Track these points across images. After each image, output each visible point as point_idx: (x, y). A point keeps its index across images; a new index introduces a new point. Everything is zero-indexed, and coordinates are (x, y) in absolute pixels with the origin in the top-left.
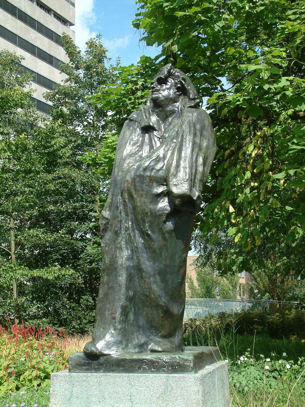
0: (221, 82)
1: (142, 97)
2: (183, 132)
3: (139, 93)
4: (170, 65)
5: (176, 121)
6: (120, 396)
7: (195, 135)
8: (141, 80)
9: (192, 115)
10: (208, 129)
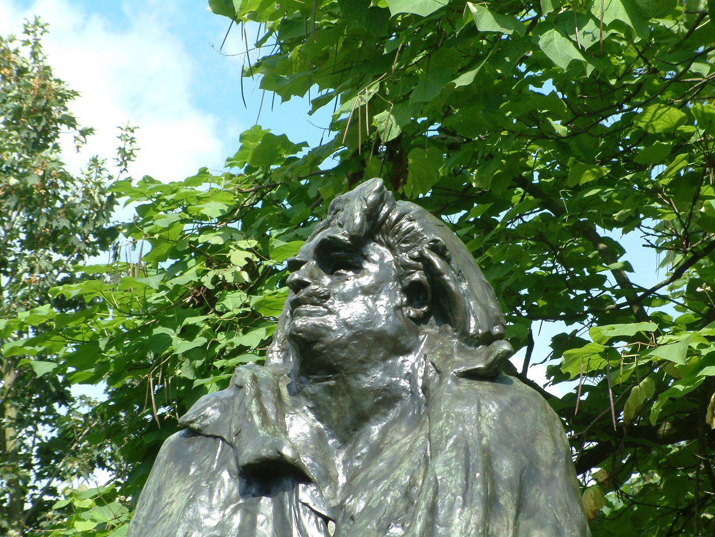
0: (622, 251)
1: (250, 320)
2: (436, 493)
3: (233, 302)
4: (378, 183)
5: (402, 439)
7: (491, 504)
8: (243, 244)
9: (477, 414)
10: (552, 478)
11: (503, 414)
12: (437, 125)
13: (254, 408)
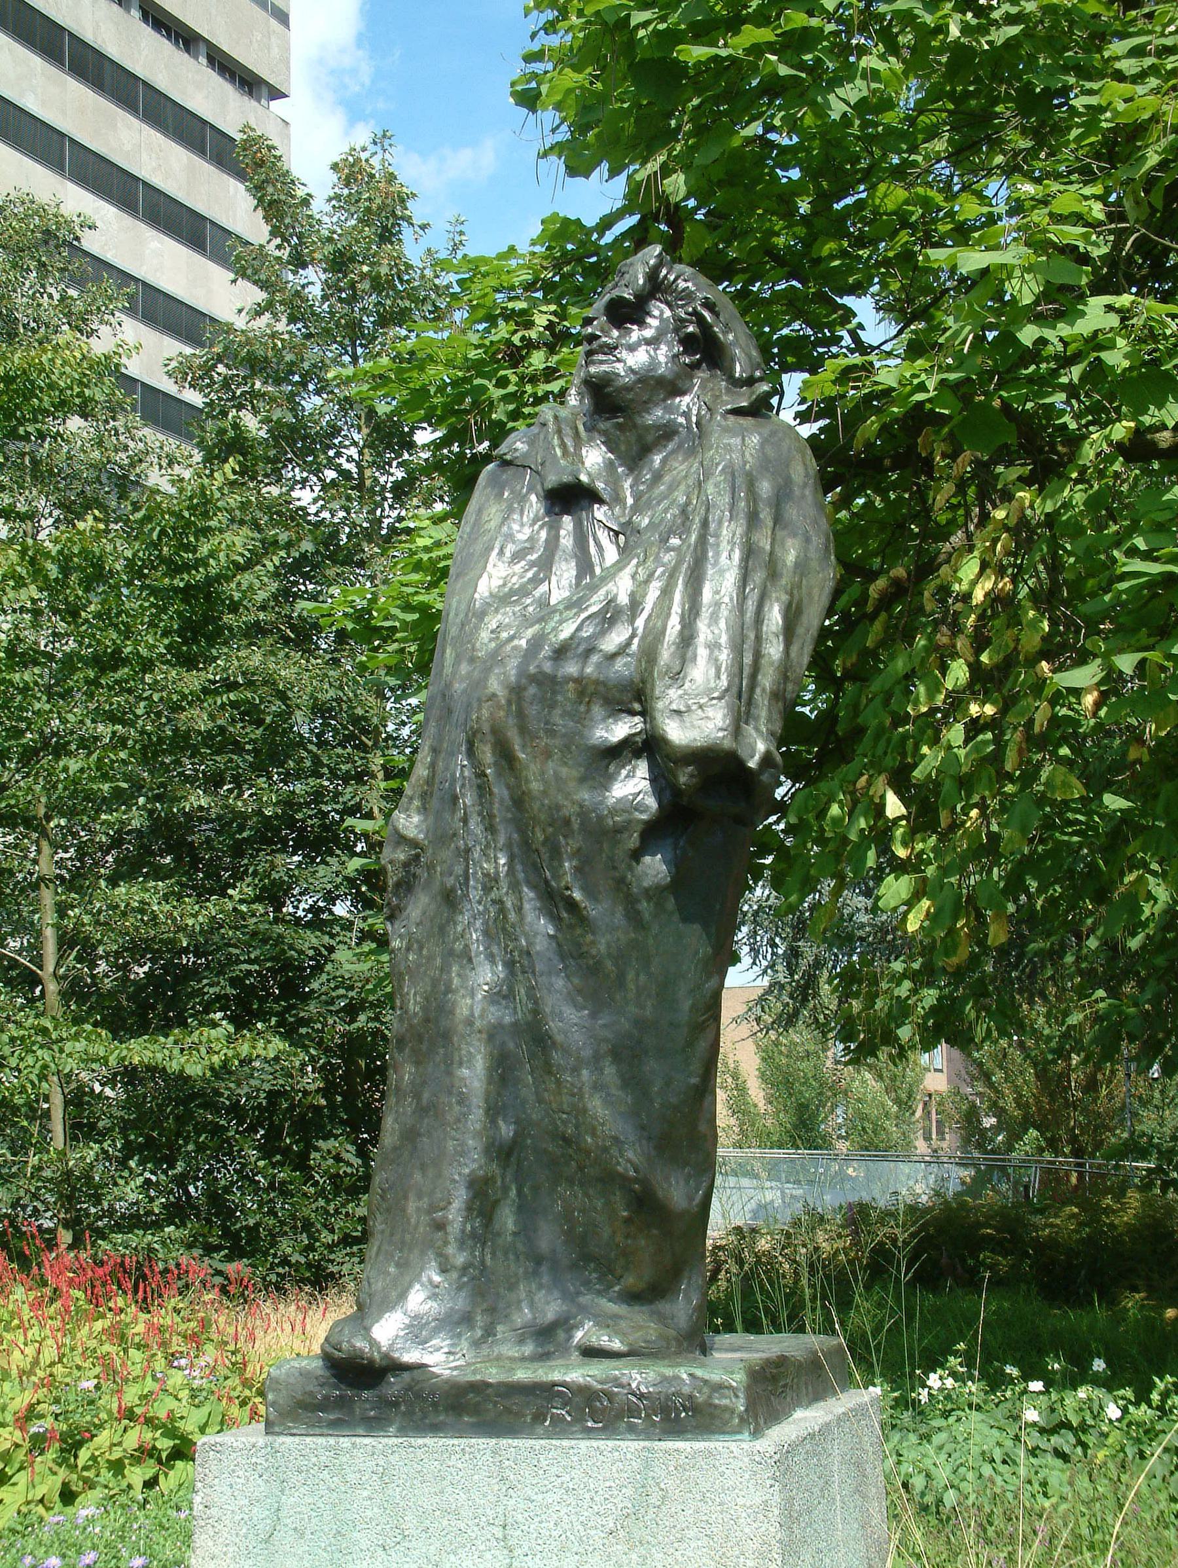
0: (855, 315)
2: (708, 510)
3: (538, 360)
4: (657, 249)
6: (462, 1526)
7: (753, 519)
8: (544, 308)
9: (740, 445)
10: (803, 497)
11: (762, 444)
12: (703, 211)
13: (556, 441)
